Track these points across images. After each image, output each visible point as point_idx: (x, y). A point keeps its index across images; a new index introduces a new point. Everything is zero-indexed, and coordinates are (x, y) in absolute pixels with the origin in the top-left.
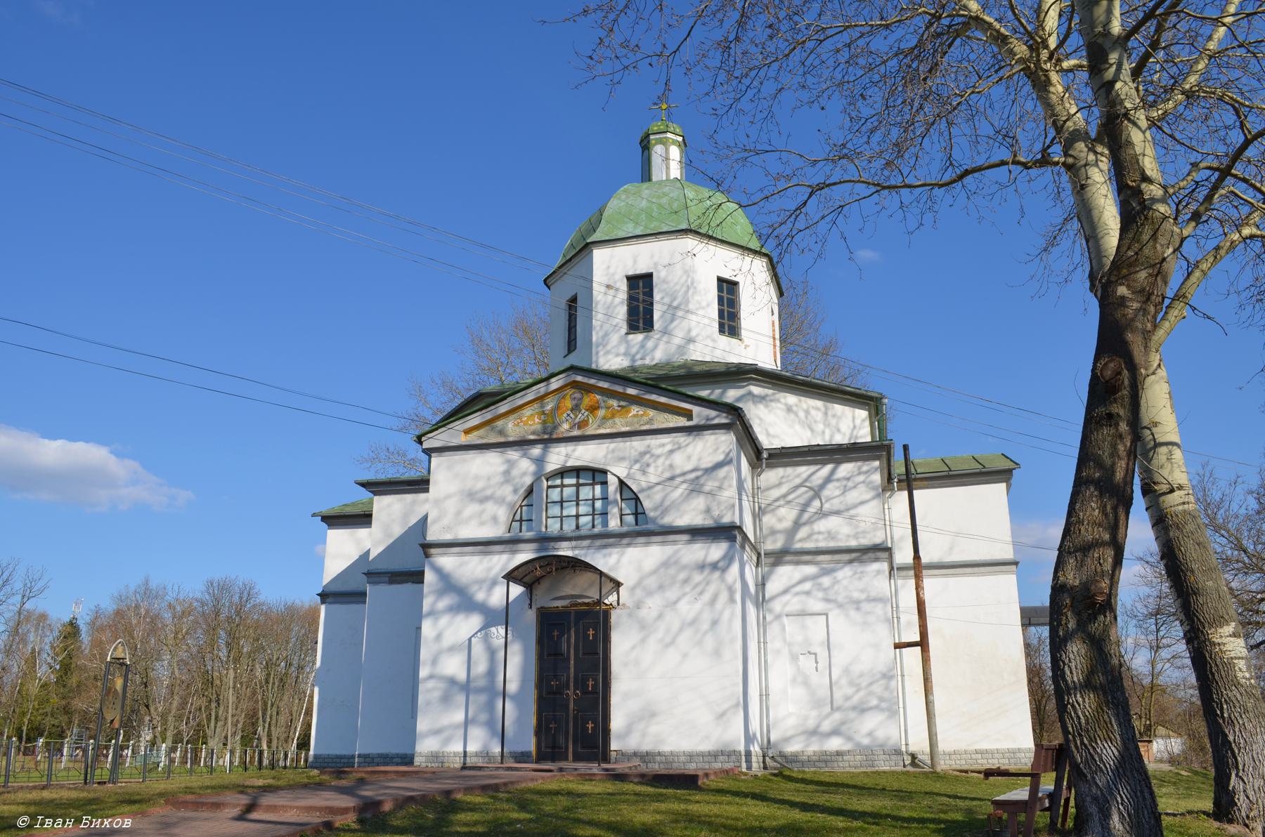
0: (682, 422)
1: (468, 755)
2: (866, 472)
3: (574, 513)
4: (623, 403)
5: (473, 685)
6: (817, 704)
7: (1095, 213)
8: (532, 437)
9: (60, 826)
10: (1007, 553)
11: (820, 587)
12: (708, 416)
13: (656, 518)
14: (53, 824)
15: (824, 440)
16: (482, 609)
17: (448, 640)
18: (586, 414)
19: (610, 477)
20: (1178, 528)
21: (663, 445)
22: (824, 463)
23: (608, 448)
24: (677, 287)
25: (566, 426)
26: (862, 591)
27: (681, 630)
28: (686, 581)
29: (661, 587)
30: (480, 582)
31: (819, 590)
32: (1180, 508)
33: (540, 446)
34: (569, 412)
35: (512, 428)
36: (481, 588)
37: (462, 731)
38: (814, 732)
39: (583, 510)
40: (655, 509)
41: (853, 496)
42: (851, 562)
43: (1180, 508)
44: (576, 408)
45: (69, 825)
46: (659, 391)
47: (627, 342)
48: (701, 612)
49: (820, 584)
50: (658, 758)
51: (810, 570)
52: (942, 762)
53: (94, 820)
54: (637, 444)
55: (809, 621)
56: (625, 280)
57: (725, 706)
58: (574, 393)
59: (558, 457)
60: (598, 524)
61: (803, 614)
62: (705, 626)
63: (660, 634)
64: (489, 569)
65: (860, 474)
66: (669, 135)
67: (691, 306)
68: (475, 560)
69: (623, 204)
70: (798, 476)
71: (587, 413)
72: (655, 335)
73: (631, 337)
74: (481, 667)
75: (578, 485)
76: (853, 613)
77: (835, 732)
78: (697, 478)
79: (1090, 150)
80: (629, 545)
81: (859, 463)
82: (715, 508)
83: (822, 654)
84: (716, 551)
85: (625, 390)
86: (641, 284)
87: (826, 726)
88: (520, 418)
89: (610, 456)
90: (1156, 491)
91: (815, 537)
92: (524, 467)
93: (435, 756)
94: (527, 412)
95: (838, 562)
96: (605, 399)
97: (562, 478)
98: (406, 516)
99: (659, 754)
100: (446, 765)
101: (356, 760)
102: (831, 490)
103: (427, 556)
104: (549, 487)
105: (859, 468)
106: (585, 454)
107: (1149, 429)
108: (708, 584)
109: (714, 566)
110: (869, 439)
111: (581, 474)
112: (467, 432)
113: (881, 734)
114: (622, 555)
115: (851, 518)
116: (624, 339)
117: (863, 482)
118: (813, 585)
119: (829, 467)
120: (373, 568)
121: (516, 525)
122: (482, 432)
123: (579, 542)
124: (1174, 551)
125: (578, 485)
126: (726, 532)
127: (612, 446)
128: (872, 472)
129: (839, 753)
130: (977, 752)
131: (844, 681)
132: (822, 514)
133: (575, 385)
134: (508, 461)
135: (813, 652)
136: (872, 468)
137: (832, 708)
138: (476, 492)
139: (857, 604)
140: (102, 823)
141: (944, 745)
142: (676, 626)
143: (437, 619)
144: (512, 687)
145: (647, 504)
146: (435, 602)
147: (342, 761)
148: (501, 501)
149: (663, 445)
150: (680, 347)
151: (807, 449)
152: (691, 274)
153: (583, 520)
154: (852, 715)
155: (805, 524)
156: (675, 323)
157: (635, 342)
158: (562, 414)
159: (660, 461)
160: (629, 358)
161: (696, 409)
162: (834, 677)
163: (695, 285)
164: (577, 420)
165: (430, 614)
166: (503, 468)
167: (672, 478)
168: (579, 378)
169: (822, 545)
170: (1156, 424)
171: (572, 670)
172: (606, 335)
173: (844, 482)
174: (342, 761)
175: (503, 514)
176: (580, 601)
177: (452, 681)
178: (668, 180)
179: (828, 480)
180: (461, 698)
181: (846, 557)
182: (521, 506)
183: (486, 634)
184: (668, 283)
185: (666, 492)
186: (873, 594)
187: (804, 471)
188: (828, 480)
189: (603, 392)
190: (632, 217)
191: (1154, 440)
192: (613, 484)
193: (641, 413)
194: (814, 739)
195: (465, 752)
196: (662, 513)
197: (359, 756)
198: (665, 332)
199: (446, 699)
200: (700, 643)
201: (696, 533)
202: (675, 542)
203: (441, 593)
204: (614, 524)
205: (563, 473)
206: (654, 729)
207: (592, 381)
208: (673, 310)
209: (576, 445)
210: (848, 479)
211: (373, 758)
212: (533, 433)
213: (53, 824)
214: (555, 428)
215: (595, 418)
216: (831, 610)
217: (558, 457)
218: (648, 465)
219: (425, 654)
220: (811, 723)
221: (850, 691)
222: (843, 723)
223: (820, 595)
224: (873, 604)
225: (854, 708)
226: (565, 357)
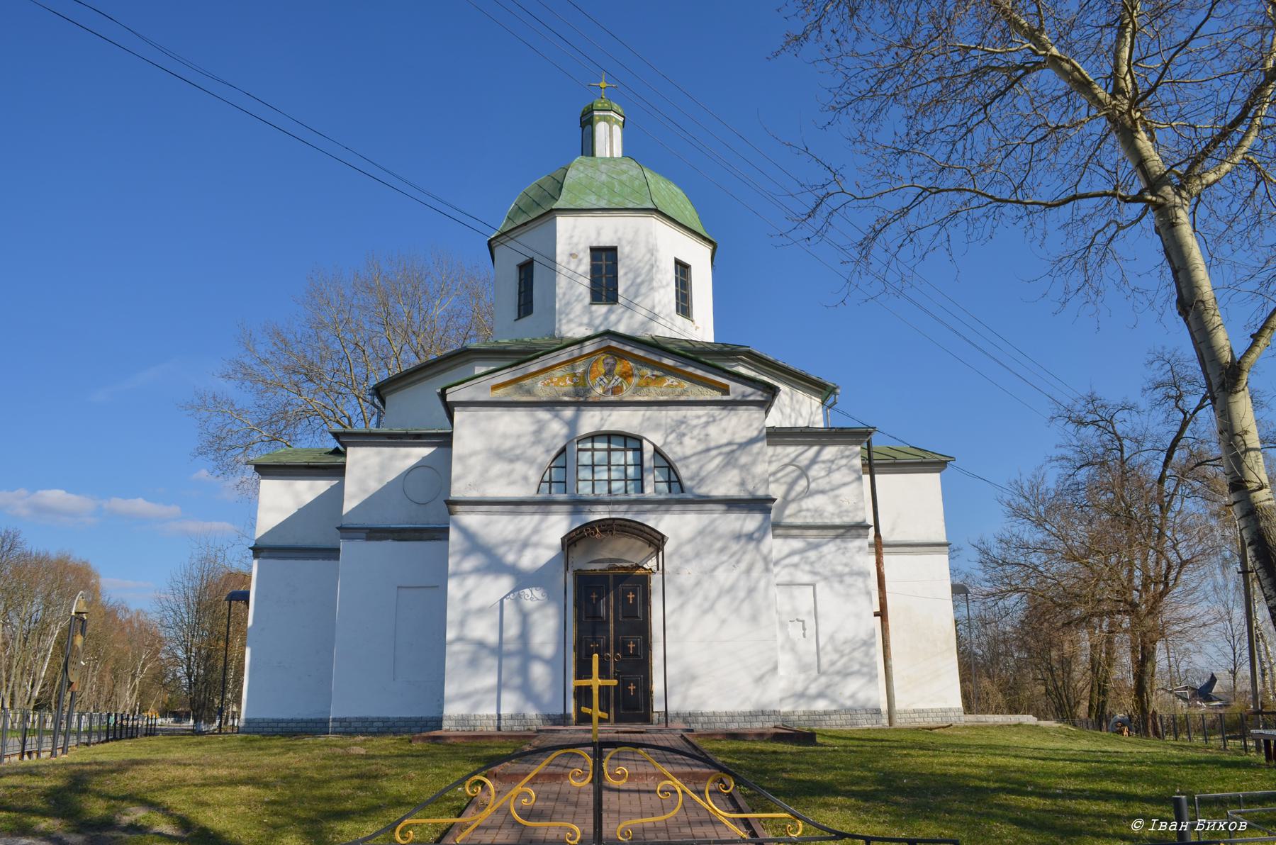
0: (717, 396)
1: (503, 717)
2: (848, 457)
3: (606, 477)
4: (656, 373)
5: (505, 648)
6: (804, 668)
7: (1186, 249)
8: (566, 399)
9: (1175, 829)
10: (943, 539)
11: (806, 560)
12: (744, 392)
13: (693, 487)
15: (790, 423)
16: (513, 570)
17: (476, 602)
18: (619, 380)
19: (645, 443)
20: (1267, 520)
21: (699, 417)
22: (811, 445)
23: (644, 415)
24: (641, 265)
25: (599, 390)
26: (846, 565)
27: (719, 596)
28: (722, 550)
29: (698, 555)
30: (506, 542)
31: (806, 563)
32: (1267, 503)
33: (573, 408)
34: (602, 377)
35: (542, 389)
36: (510, 550)
37: (495, 696)
38: (801, 695)
39: (614, 475)
40: (692, 479)
41: (837, 477)
42: (837, 537)
43: (1267, 503)
44: (609, 373)
46: (697, 364)
47: (591, 312)
48: (738, 580)
49: (807, 558)
50: (701, 719)
51: (797, 544)
52: (899, 721)
54: (673, 414)
55: (797, 591)
56: (589, 251)
57: (764, 669)
58: (607, 358)
59: (592, 421)
60: (631, 490)
61: (790, 584)
62: (742, 594)
63: (698, 600)
64: (519, 531)
65: (842, 457)
66: (612, 114)
67: (655, 284)
68: (504, 519)
69: (582, 175)
70: (788, 455)
71: (620, 380)
72: (618, 309)
73: (595, 307)
74: (512, 631)
75: (609, 450)
76: (836, 585)
77: (821, 695)
78: (733, 451)
79: (1176, 193)
80: (667, 511)
81: (842, 447)
82: (750, 481)
83: (810, 623)
84: (751, 522)
85: (660, 359)
86: (604, 257)
87: (813, 689)
88: (551, 379)
89: (646, 424)
90: (1247, 488)
91: (804, 513)
92: (556, 429)
93: (463, 720)
94: (558, 373)
95: (823, 537)
96: (639, 367)
97: (593, 442)
98: (383, 467)
99: (702, 714)
100: (479, 728)
101: (331, 724)
102: (815, 471)
103: (451, 513)
104: (579, 450)
105: (842, 452)
106: (620, 420)
107: (1240, 436)
108: (744, 553)
109: (750, 537)
110: (822, 425)
111: (613, 439)
112: (495, 387)
113: (862, 696)
114: (660, 520)
115: (837, 496)
116: (586, 310)
117: (846, 465)
118: (802, 559)
119: (815, 449)
120: (345, 523)
121: (545, 486)
122: (509, 389)
123: (616, 506)
124: (1265, 539)
125: (609, 450)
126: (759, 504)
127: (648, 413)
128: (854, 455)
129: (826, 713)
130: (914, 711)
131: (829, 648)
132: (808, 493)
133: (608, 350)
134: (539, 421)
135: (801, 619)
136: (854, 453)
137: (819, 672)
138: (505, 452)
139: (840, 577)
140: (1217, 825)
141: (899, 705)
142: (713, 593)
143: (464, 579)
144: (548, 650)
145: (684, 473)
146: (459, 563)
147: (280, 725)
148: (531, 461)
149: (699, 417)
150: (643, 324)
151: (799, 430)
152: (655, 253)
153: (615, 485)
154: (837, 679)
155: (793, 500)
157: (598, 313)
158: (595, 378)
159: (696, 432)
160: (593, 329)
161: (733, 385)
162: (821, 644)
163: (658, 263)
164: (610, 386)
165: (455, 574)
166: (533, 428)
167: (708, 450)
168: (614, 344)
169: (810, 521)
170: (1246, 432)
171: (612, 632)
172: (568, 304)
173: (829, 464)
174: (280, 725)
175: (534, 477)
176: (619, 565)
177: (481, 644)
178: (612, 157)
179: (814, 461)
180: (492, 662)
181: (832, 533)
182: (550, 468)
183: (519, 596)
184: (632, 259)
185: (701, 463)
186: (855, 568)
187: (792, 450)
188: (814, 461)
189: (637, 359)
190: (593, 190)
191: (1246, 445)
192: (648, 452)
193: (675, 383)
194: (802, 701)
195: (499, 716)
196: (698, 483)
197: (334, 720)
199: (474, 663)
200: (737, 610)
201: (732, 504)
202: (712, 511)
203: (466, 553)
204: (649, 491)
205: (593, 437)
206: (695, 691)
207: (628, 348)
208: (636, 287)
209: (612, 410)
210: (832, 462)
211: (350, 723)
212: (565, 395)
213: (1168, 826)
214: (589, 391)
215: (630, 385)
216: (817, 581)
217: (592, 421)
218: (684, 435)
219: (452, 615)
220: (799, 687)
221: (835, 657)
222: (828, 686)
223: (807, 568)
224: (855, 578)
225: (838, 673)
226: (515, 320)
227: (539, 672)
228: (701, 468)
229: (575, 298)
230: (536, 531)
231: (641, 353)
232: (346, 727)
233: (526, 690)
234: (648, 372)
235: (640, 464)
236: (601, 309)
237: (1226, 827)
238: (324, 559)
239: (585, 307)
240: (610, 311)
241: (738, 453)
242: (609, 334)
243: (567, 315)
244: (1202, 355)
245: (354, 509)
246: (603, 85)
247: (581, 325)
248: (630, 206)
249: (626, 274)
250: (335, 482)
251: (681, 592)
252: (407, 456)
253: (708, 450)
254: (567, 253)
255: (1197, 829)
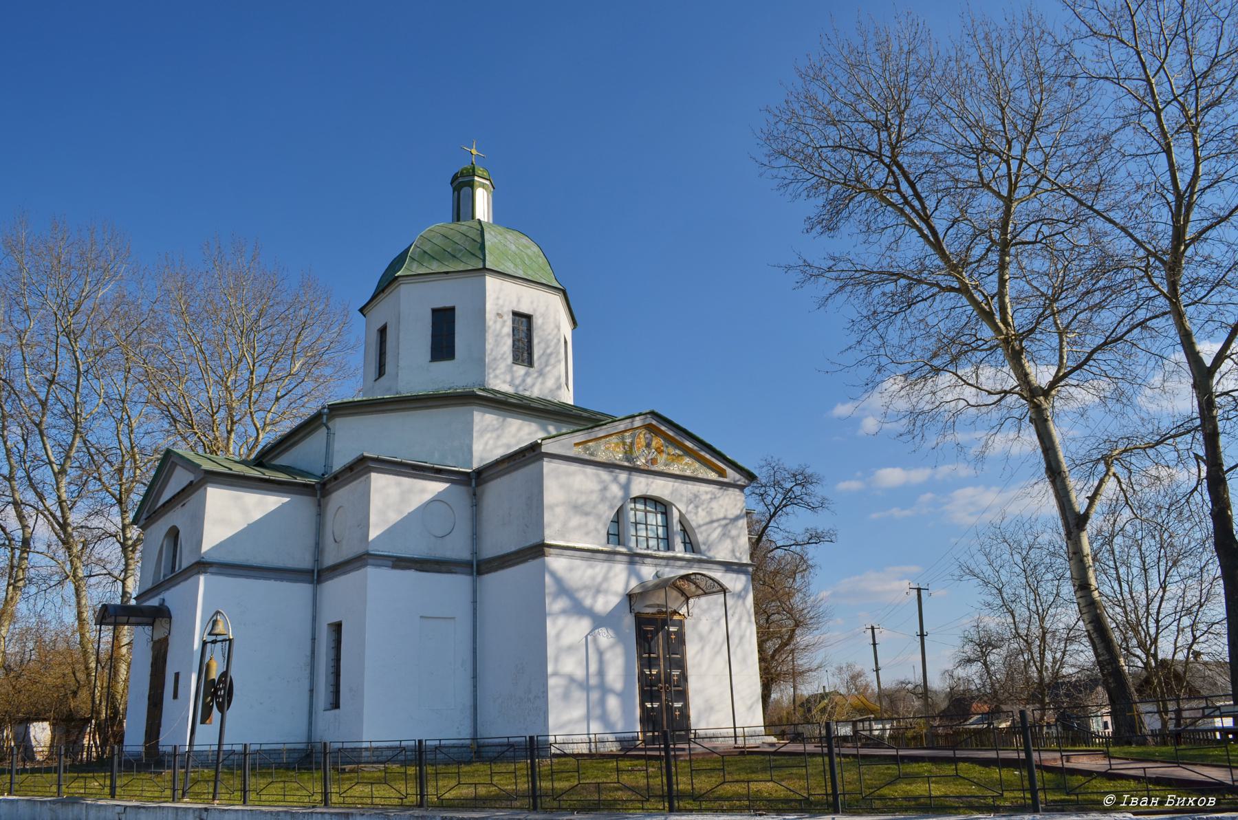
4: (677, 451)
9: (1146, 805)
14: (1139, 802)
24: (550, 337)
30: (586, 588)
45: (1154, 803)
53: (1179, 799)
59: (641, 485)
73: (516, 367)
74: (593, 668)
75: (646, 512)
78: (727, 525)
97: (635, 503)
106: (659, 488)
116: (510, 370)
127: (676, 484)
140: (1187, 801)
144: (618, 685)
150: (551, 391)
156: (548, 368)
161: (729, 471)
167: (712, 522)
177: (571, 679)
180: (578, 695)
184: (544, 330)
198: (541, 373)
199: (566, 696)
205: (645, 499)
207: (663, 428)
213: (1139, 802)
217: (641, 485)
227: (613, 703)
228: (709, 535)
229: (500, 356)
230: (606, 578)
231: (671, 433)
232: (378, 757)
233: (604, 718)
234: (672, 451)
235: (667, 526)
236: (521, 370)
237: (1196, 802)
238: (276, 579)
239: (508, 366)
240: (527, 374)
241: (730, 527)
242: (654, 414)
243: (494, 370)
244: (1064, 504)
245: (378, 537)
246: (474, 151)
247: (504, 382)
248: (544, 282)
249: (539, 343)
250: (286, 500)
251: (701, 638)
252: (423, 491)
253: (712, 522)
254: (495, 312)
255: (1167, 805)
